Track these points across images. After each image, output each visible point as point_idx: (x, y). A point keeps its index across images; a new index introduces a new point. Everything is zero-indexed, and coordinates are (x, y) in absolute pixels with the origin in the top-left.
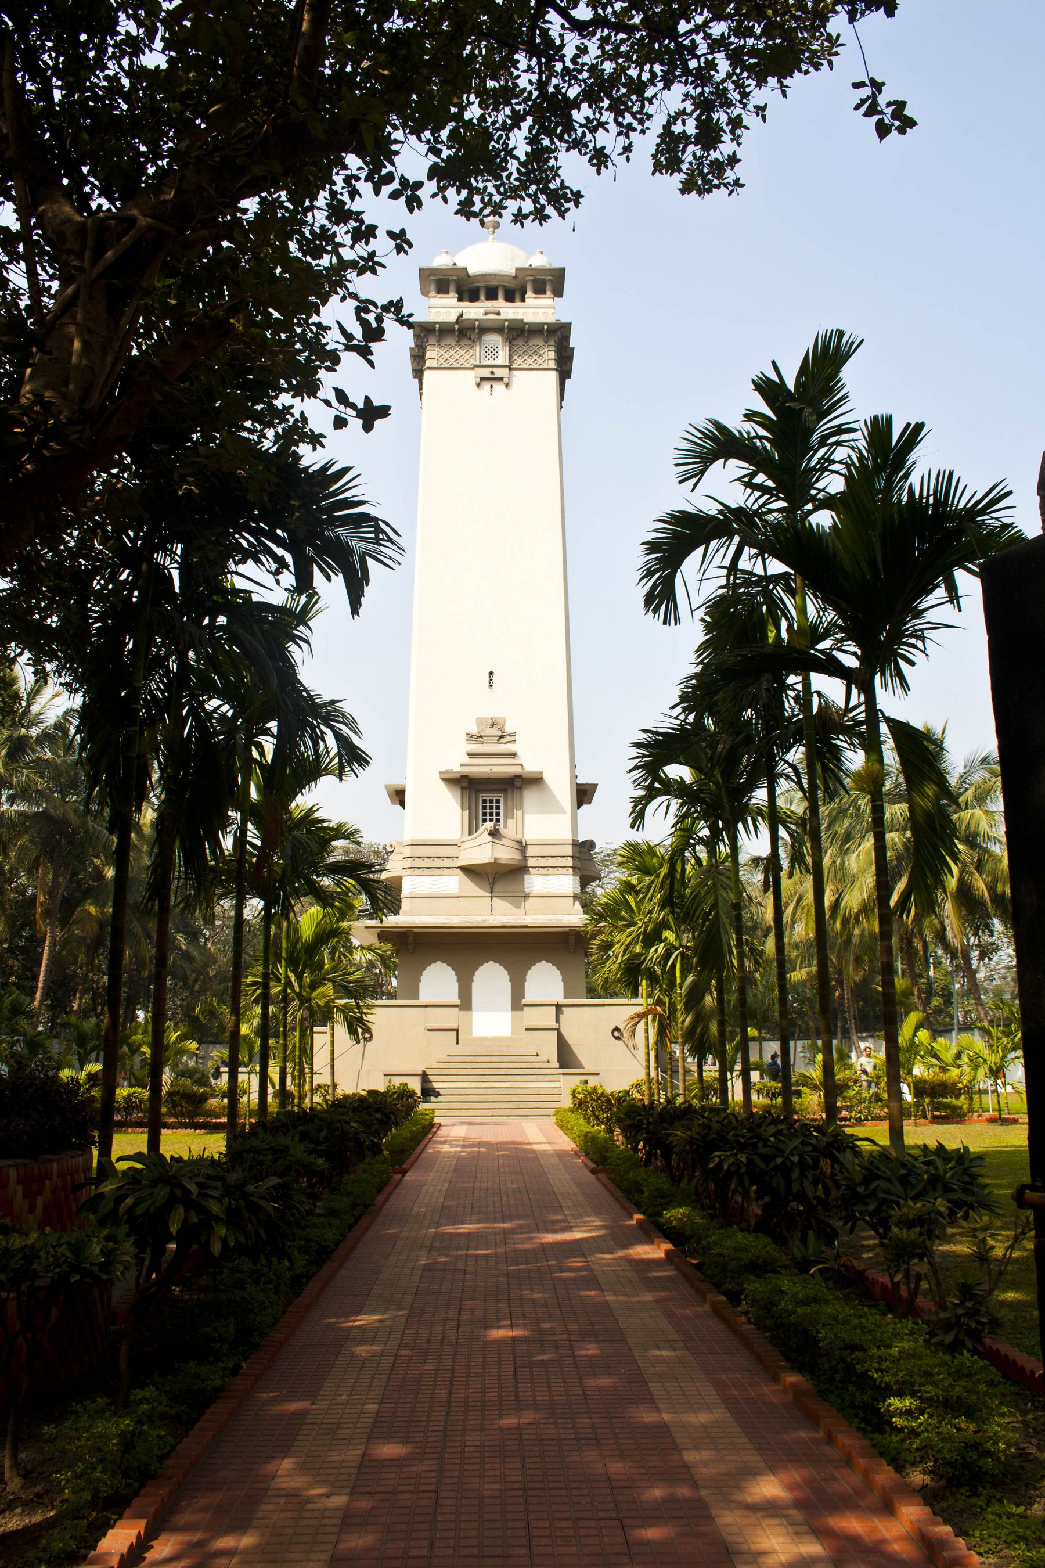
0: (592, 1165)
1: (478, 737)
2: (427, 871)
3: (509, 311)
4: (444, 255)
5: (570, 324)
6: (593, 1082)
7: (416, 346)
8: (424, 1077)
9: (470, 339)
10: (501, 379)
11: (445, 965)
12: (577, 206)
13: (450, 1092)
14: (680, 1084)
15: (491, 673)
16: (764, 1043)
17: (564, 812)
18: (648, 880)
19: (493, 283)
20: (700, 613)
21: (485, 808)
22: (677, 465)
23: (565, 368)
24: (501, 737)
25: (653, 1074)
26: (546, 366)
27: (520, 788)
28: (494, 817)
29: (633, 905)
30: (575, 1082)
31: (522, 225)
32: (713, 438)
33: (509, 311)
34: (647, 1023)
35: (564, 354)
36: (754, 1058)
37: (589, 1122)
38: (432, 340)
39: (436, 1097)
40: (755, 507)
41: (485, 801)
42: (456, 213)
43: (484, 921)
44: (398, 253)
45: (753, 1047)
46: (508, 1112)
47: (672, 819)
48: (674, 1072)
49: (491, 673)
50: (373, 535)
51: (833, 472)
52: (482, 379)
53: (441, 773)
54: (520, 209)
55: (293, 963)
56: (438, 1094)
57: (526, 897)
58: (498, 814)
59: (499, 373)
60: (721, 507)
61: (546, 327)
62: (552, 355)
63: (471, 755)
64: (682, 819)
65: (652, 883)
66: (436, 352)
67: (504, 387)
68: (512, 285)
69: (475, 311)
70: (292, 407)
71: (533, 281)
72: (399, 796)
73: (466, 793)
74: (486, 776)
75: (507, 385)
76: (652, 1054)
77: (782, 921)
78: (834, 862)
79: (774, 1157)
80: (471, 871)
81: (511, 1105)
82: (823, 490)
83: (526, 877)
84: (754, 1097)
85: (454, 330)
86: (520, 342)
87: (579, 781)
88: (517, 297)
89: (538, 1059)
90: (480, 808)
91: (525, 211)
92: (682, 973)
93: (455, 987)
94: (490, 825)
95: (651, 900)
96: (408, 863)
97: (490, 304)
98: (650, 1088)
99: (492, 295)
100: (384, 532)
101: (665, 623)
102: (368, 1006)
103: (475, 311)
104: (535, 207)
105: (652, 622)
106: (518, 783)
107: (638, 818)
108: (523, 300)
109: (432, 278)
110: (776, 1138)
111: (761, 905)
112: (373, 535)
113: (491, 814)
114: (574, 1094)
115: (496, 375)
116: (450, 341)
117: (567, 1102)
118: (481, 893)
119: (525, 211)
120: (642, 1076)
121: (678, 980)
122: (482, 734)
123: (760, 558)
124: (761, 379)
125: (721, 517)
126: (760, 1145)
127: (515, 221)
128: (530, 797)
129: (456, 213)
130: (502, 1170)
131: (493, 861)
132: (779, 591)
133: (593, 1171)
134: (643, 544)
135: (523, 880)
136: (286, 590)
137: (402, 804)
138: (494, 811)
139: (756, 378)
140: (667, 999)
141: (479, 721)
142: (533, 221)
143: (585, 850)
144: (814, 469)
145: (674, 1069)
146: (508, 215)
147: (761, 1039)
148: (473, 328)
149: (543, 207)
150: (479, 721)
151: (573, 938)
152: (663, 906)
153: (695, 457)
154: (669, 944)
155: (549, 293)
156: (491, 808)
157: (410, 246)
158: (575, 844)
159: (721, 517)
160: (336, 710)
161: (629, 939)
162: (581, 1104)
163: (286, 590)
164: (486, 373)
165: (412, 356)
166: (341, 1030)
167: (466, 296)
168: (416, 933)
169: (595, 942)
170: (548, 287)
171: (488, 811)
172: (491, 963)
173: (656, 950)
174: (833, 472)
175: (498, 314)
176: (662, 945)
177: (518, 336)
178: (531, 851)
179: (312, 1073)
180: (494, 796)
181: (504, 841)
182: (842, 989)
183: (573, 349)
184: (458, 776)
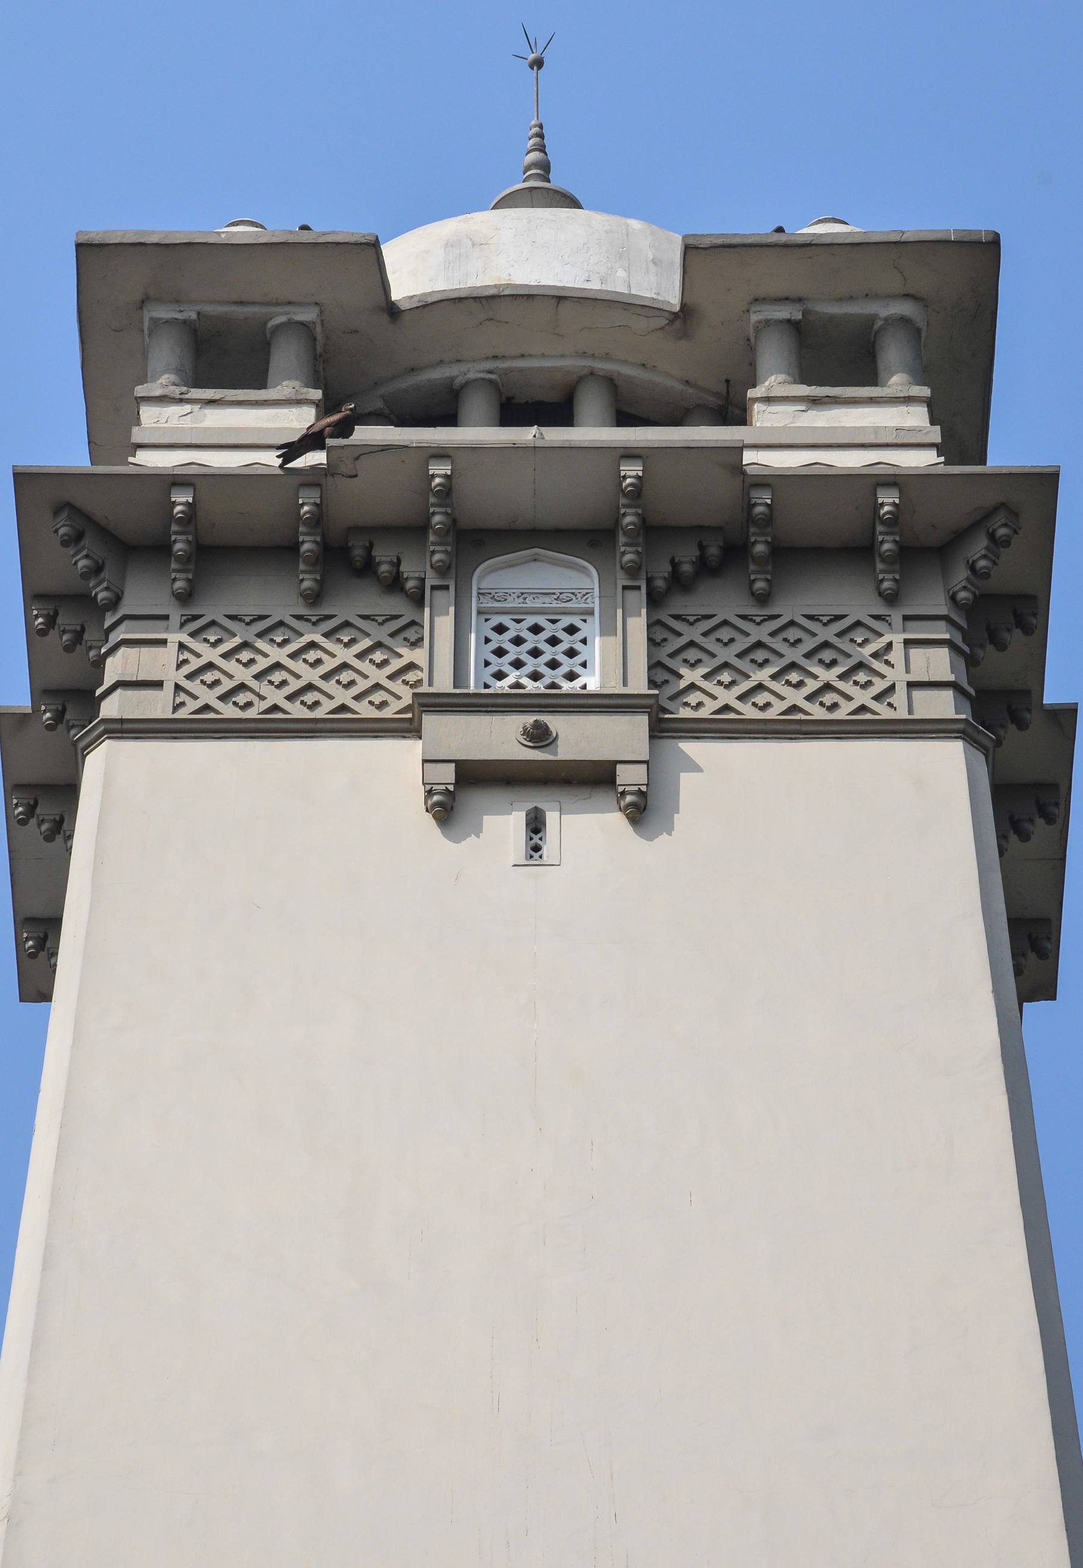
9: (394, 584)
67: (617, 820)
177: (706, 569)
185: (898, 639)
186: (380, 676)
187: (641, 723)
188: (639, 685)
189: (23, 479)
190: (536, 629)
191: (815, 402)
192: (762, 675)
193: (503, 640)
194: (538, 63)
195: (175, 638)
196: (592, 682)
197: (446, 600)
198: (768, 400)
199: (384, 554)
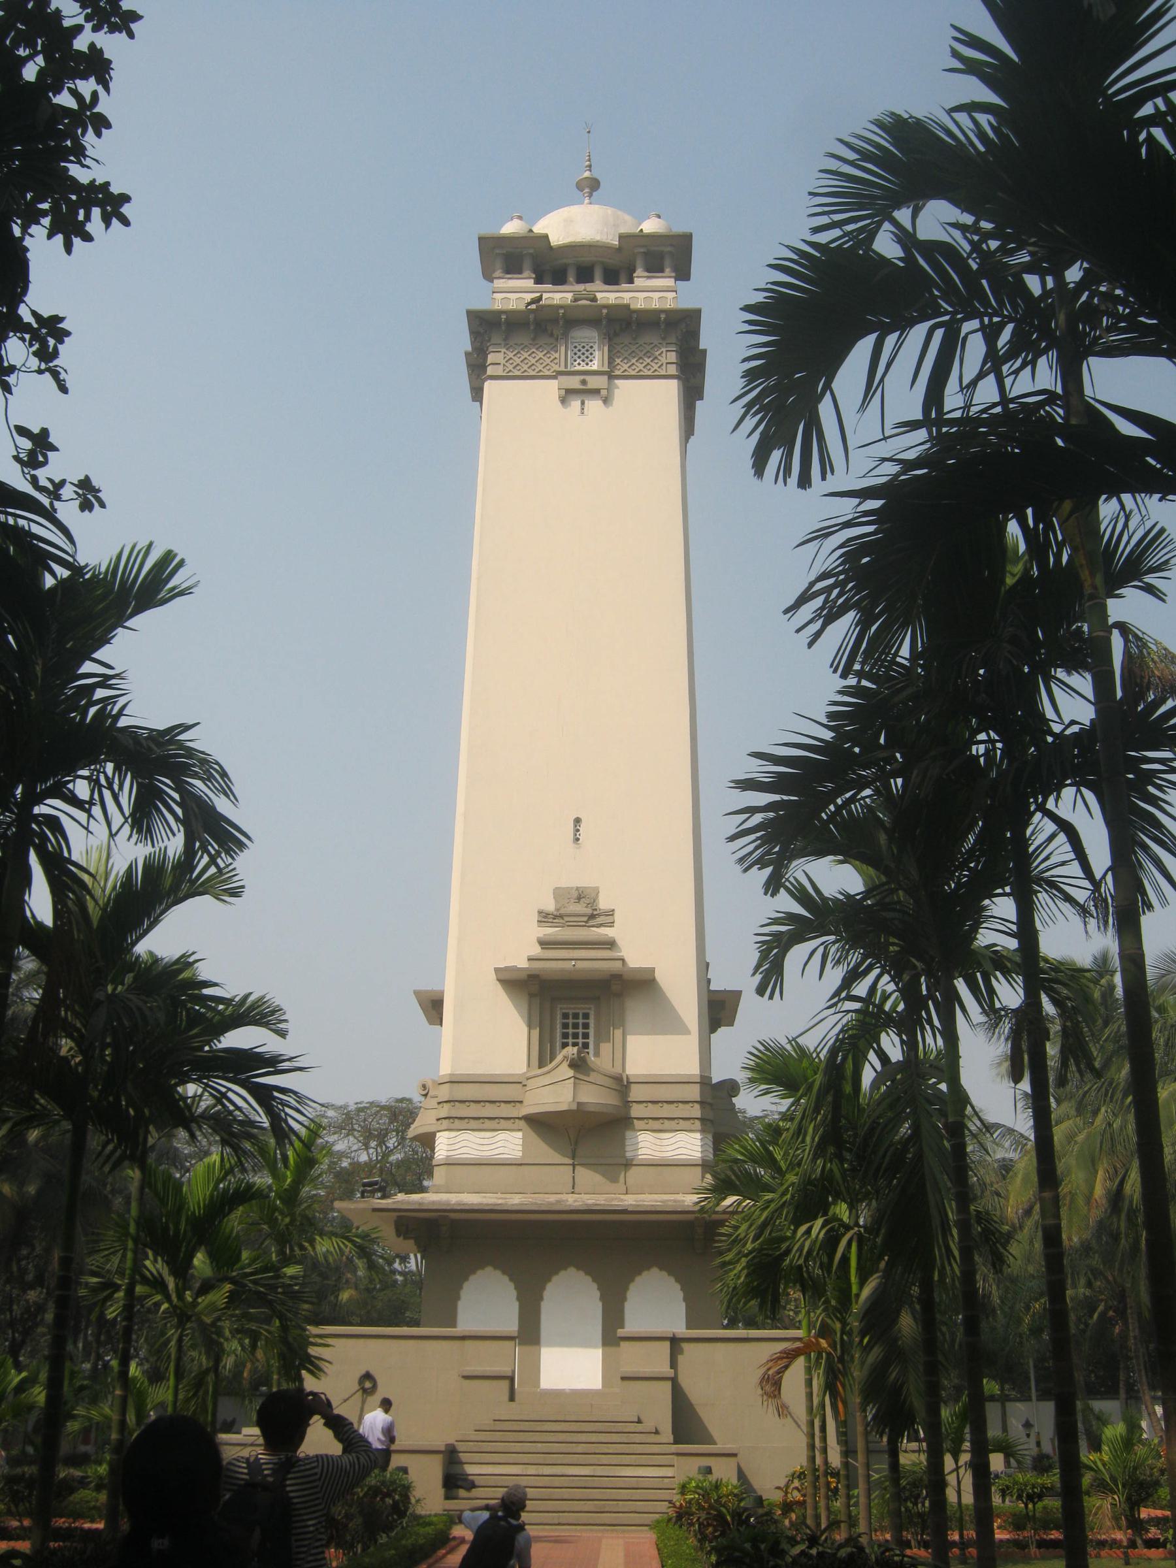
1: (555, 917)
2: (474, 1124)
3: (608, 296)
9: (552, 335)
15: (578, 821)
16: (1008, 1404)
17: (686, 1031)
21: (565, 1026)
26: (663, 373)
27: (619, 995)
28: (580, 1041)
30: (686, 1469)
32: (882, 159)
33: (608, 296)
34: (808, 1370)
36: (993, 1432)
38: (496, 338)
39: (469, 1489)
41: (565, 1016)
43: (558, 1202)
45: (992, 1412)
49: (578, 821)
53: (497, 970)
56: (472, 1486)
57: (628, 1164)
58: (586, 1036)
59: (594, 382)
61: (663, 316)
62: (673, 357)
63: (544, 943)
66: (501, 355)
67: (600, 403)
69: (558, 296)
71: (645, 254)
72: (433, 1007)
75: (606, 401)
78: (1110, 1125)
81: (589, 1506)
83: (629, 1134)
84: (996, 1500)
87: (712, 987)
88: (623, 276)
89: (639, 1427)
93: (515, 1307)
94: (571, 1051)
96: (445, 1111)
99: (585, 275)
103: (558, 296)
108: (631, 281)
111: (998, 1194)
115: (590, 386)
118: (557, 1158)
121: (855, 1289)
122: (562, 911)
128: (635, 1010)
131: (574, 1107)
135: (623, 1139)
140: (838, 1326)
141: (558, 893)
147: (1004, 1399)
148: (555, 321)
150: (558, 893)
152: (820, 1150)
155: (668, 270)
156: (576, 1026)
158: (705, 1081)
164: (574, 382)
168: (453, 1221)
170: (667, 262)
171: (571, 1031)
173: (808, 1232)
175: (594, 299)
178: (636, 1093)
181: (593, 1077)
182: (1126, 1323)
183: (704, 351)
184: (523, 976)
185: (664, 350)
186: (548, 361)
187: (606, 377)
188: (606, 369)
190: (583, 347)
191: (648, 277)
192: (634, 361)
193: (576, 350)
194: (589, 132)
195: (503, 350)
196: (595, 368)
198: (638, 277)
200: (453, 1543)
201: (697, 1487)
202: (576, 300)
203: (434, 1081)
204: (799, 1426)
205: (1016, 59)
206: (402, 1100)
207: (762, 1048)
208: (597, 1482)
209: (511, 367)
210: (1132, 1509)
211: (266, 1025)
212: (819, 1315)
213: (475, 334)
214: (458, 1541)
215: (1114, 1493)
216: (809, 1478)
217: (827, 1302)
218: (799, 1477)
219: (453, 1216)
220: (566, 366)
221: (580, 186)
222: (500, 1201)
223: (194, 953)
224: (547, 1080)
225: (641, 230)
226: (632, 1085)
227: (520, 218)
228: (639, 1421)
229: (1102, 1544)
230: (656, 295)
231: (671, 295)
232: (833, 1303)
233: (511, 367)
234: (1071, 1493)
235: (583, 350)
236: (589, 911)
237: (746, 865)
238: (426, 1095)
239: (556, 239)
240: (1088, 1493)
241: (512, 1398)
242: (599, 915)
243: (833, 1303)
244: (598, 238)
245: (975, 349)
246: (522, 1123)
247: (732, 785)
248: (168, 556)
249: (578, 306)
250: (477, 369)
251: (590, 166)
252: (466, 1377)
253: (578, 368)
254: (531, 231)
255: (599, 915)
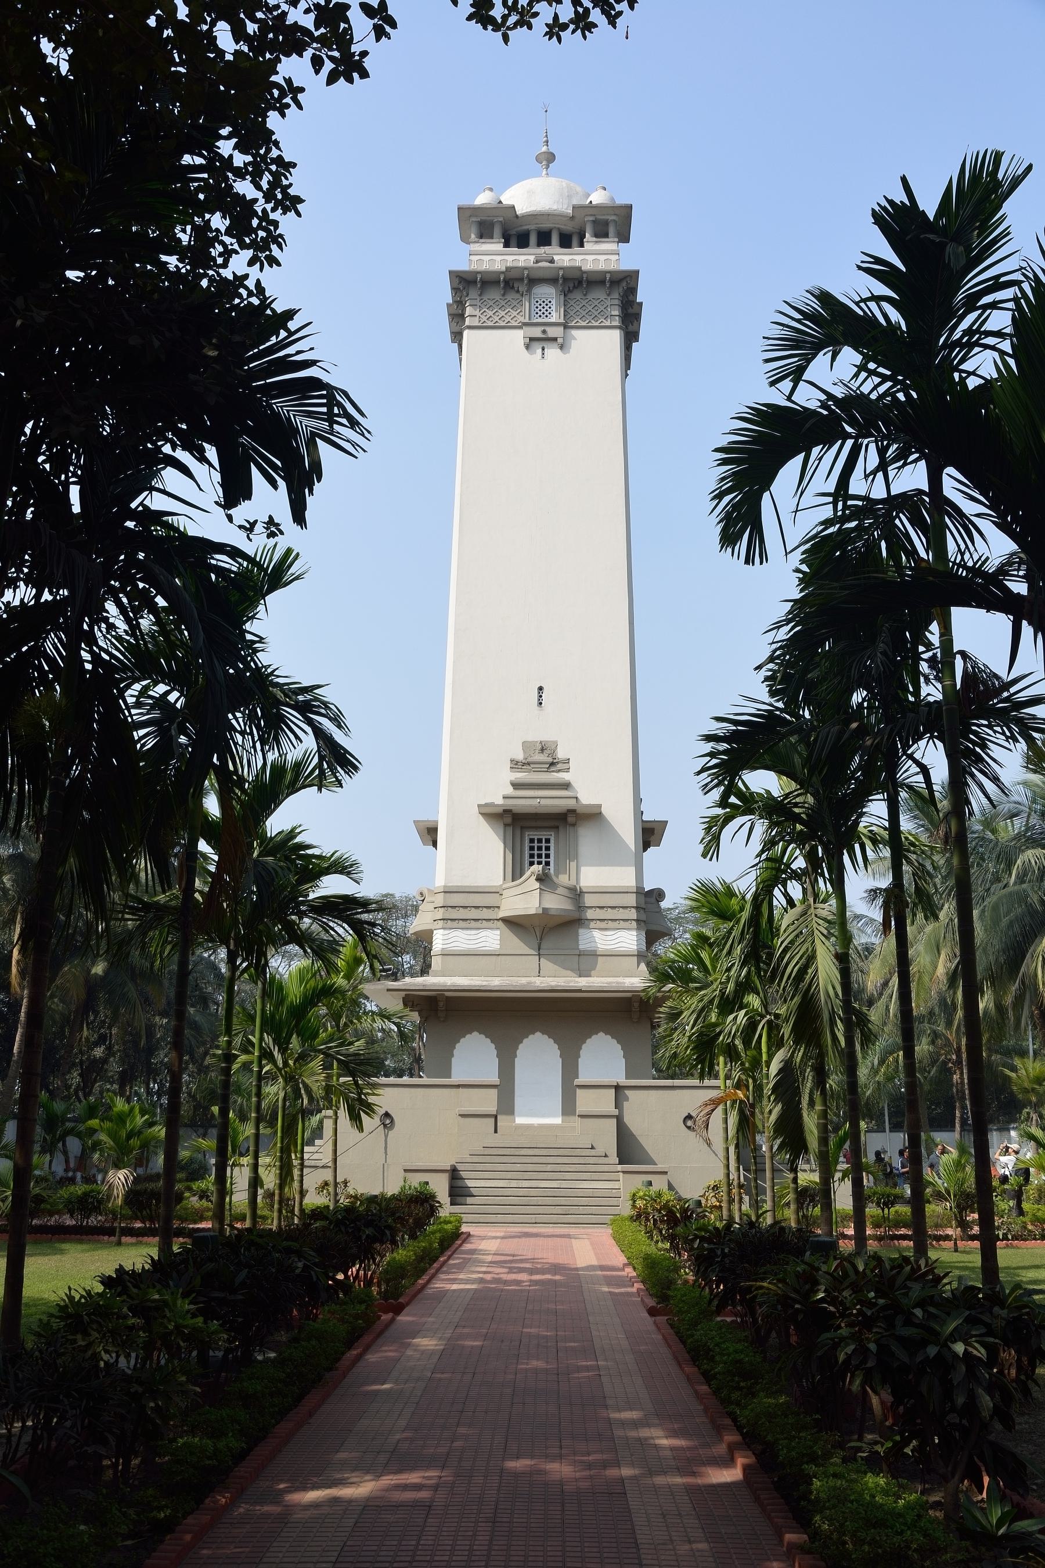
0: (651, 1302)
1: (524, 764)
3: (565, 259)
4: (487, 192)
5: (637, 272)
6: (659, 1184)
7: (455, 302)
8: (454, 1174)
9: (518, 291)
10: (555, 339)
11: (483, 1036)
12: (632, 8)
13: (484, 1192)
14: (768, 1185)
15: (541, 689)
18: (725, 926)
19: (546, 226)
20: (797, 556)
21: (532, 848)
22: (767, 361)
23: (631, 328)
24: (552, 764)
25: (733, 1176)
27: (574, 825)
28: (543, 860)
29: (708, 963)
31: (559, 40)
33: (565, 259)
34: (726, 1111)
35: (630, 311)
37: (651, 1237)
38: (474, 293)
40: (874, 396)
41: (532, 841)
42: (469, 19)
44: (378, 39)
46: (554, 1218)
47: (756, 845)
48: (760, 1171)
49: (541, 689)
50: (324, 410)
51: (986, 347)
52: (532, 339)
53: (479, 806)
54: (556, 17)
55: (270, 1024)
58: (548, 856)
59: (552, 332)
60: (823, 397)
63: (516, 786)
64: (769, 844)
65: (730, 932)
68: (568, 227)
69: (524, 258)
70: (246, 276)
71: (594, 222)
72: (430, 834)
73: (510, 830)
74: (532, 811)
76: (732, 1149)
77: (908, 972)
79: (924, 1343)
80: (513, 923)
81: (558, 1210)
82: (974, 373)
83: (581, 931)
85: (498, 282)
86: (577, 295)
88: (575, 241)
89: (593, 1152)
90: (527, 848)
91: (563, 20)
92: (769, 1049)
94: (537, 868)
95: (729, 953)
96: (440, 913)
97: (543, 250)
98: (729, 1192)
99: (544, 239)
100: (340, 406)
101: (747, 562)
102: (375, 1086)
103: (524, 258)
104: (576, 12)
105: (731, 562)
106: (571, 819)
107: (712, 845)
108: (582, 245)
109: (474, 219)
110: (925, 1311)
112: (324, 410)
113: (540, 856)
114: (634, 1198)
116: (495, 294)
117: (627, 1210)
119: (563, 20)
120: (720, 1175)
121: (764, 1057)
122: (530, 760)
123: (880, 475)
124: (884, 208)
125: (825, 413)
126: (899, 1321)
127: (550, 34)
128: (586, 839)
129: (469, 19)
130: (530, 1307)
132: (903, 522)
133: (652, 1312)
134: (717, 450)
135: (577, 935)
136: (240, 527)
137: (435, 844)
138: (544, 852)
139: (877, 208)
141: (526, 745)
142: (573, 32)
143: (653, 900)
144: (958, 343)
145: (759, 1166)
146: (540, 24)
148: (521, 280)
149: (587, 11)
150: (526, 745)
151: (636, 1005)
153: (792, 348)
154: (753, 1010)
156: (540, 848)
157: (394, 25)
158: (640, 892)
159: (825, 413)
160: (316, 699)
161: (701, 1005)
162: (639, 1216)
163: (240, 527)
164: (537, 332)
165: (450, 315)
166: (343, 1114)
167: (513, 241)
169: (661, 1010)
170: (612, 230)
171: (536, 852)
172: (538, 1034)
174: (986, 347)
175: (552, 261)
176: (743, 1012)
177: (575, 287)
178: (589, 900)
179: (302, 1166)
180: (543, 835)
184: (500, 810)
188: (562, 320)
189: (450, 272)
196: (553, 320)
197: (527, 297)
199: (516, 285)
200: (464, 1236)
201: (645, 1195)
202: (537, 262)
203: (429, 890)
204: (716, 1155)
205: (904, 270)
206: (386, 895)
207: (699, 885)
208: (563, 1192)
209: (485, 319)
210: (960, 1213)
211: (348, 874)
212: (737, 1074)
213: (455, 290)
214: (465, 1236)
215: (946, 1200)
216: (724, 1188)
217: (742, 1064)
218: (713, 1188)
219: (447, 994)
220: (530, 319)
221: (538, 159)
222: (484, 983)
223: (300, 826)
224: (519, 890)
225: (591, 202)
226: (586, 895)
227: (491, 189)
228: (593, 1148)
229: (938, 1238)
230: (602, 258)
231: (614, 258)
232: (747, 1065)
233: (485, 319)
234: (918, 1201)
235: (543, 305)
236: (550, 760)
237: (706, 790)
238: (423, 901)
239: (520, 210)
240: (929, 1202)
241: (496, 1131)
242: (558, 763)
243: (747, 1065)
244: (555, 207)
245: (871, 458)
246: (500, 923)
247: (700, 738)
248: (289, 551)
249: (540, 268)
250: (457, 316)
251: (547, 142)
252: (462, 1116)
253: (540, 320)
254: (500, 202)
255: (558, 763)
